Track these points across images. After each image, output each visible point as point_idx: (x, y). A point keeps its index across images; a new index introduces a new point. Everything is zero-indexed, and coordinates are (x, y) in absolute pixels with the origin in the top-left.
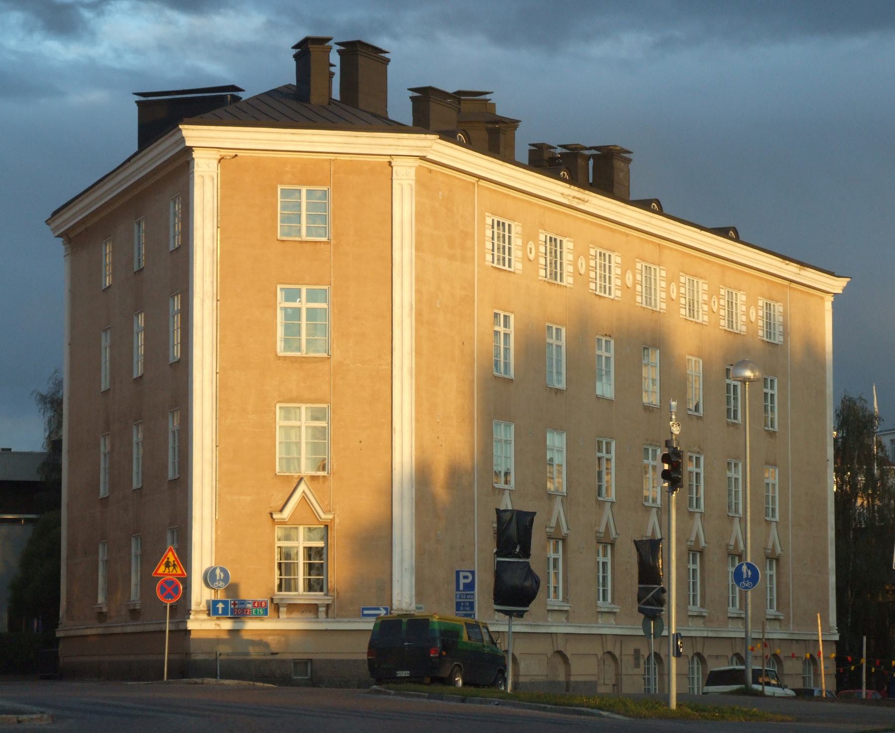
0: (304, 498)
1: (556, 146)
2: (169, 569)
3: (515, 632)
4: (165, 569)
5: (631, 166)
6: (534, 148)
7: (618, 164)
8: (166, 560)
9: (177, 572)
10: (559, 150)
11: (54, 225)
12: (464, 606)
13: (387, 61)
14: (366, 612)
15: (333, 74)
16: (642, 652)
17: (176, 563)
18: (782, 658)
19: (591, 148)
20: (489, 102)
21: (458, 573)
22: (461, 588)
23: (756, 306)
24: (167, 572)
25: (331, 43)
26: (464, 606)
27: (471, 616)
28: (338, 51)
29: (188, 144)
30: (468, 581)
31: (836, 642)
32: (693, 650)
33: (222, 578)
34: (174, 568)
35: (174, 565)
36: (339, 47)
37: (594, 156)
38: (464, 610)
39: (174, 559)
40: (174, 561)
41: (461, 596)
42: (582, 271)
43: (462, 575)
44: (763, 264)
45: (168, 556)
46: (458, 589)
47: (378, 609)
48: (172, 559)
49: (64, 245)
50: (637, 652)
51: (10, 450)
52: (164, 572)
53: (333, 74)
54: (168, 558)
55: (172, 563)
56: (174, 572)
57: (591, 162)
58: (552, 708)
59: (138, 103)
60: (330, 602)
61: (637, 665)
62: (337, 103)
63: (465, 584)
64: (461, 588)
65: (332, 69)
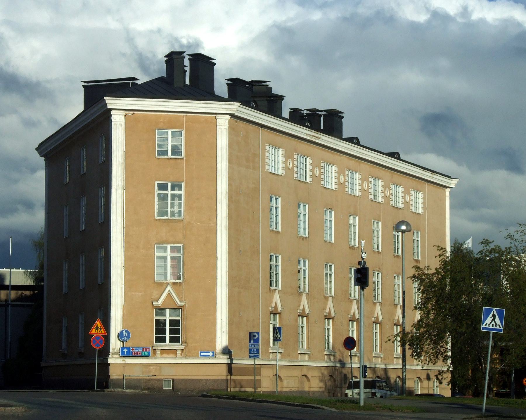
0: (169, 294)
2: (97, 331)
4: (96, 331)
8: (96, 326)
9: (102, 332)
10: (305, 112)
12: (254, 351)
14: (202, 354)
15: (186, 71)
17: (101, 327)
19: (322, 111)
20: (268, 86)
25: (185, 54)
26: (254, 351)
27: (257, 356)
29: (109, 107)
33: (126, 336)
35: (100, 329)
36: (189, 57)
37: (324, 115)
38: (254, 353)
40: (100, 327)
41: (252, 346)
47: (208, 352)
48: (99, 325)
52: (95, 332)
55: (99, 327)
56: (100, 332)
57: (322, 118)
59: (84, 86)
60: (183, 348)
65: (186, 69)
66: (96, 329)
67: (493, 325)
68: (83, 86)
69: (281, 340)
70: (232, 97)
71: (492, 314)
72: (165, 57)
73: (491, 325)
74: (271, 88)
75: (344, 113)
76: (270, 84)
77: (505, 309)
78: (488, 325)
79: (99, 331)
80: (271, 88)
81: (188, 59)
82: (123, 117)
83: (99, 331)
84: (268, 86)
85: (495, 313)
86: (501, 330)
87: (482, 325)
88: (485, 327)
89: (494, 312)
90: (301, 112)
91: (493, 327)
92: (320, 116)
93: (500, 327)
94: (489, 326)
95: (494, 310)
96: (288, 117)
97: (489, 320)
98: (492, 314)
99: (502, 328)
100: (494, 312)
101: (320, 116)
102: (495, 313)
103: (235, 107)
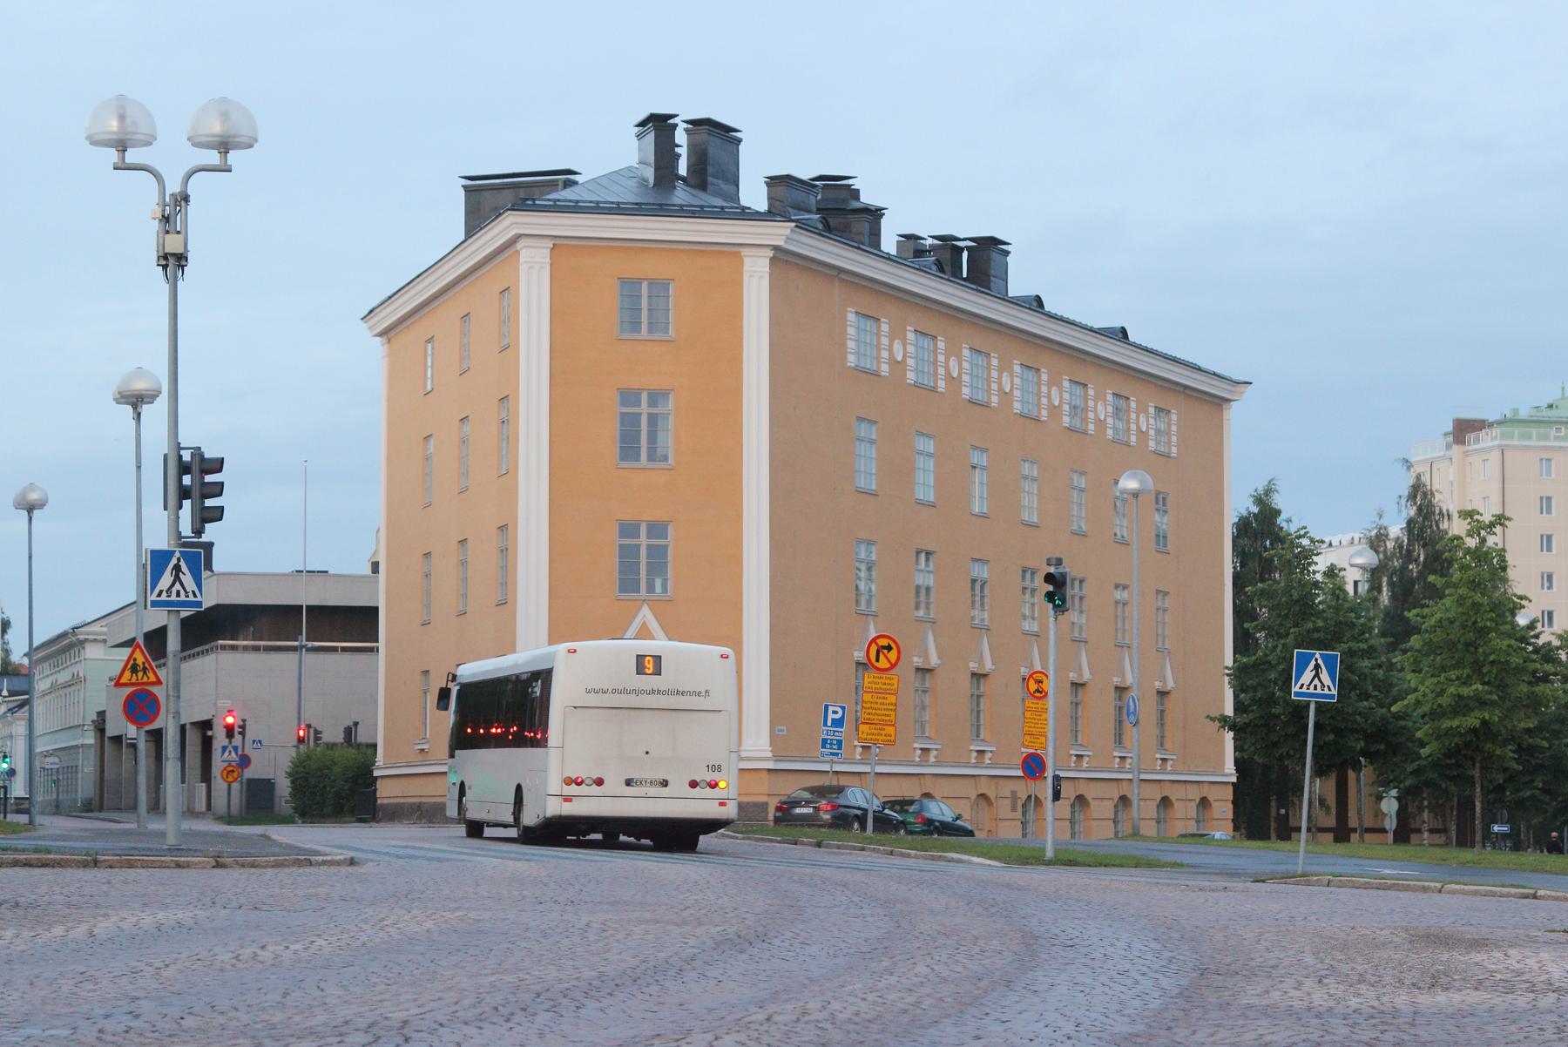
1: (926, 236)
2: (137, 676)
3: (837, 772)
4: (132, 676)
5: (1009, 259)
6: (903, 239)
7: (995, 256)
8: (132, 662)
9: (149, 679)
10: (930, 241)
11: (371, 323)
12: (831, 744)
13: (739, 141)
15: (679, 155)
16: (1019, 795)
17: (146, 665)
18: (1212, 801)
20: (853, 187)
21: (827, 707)
22: (829, 723)
23: (1105, 401)
24: (134, 680)
28: (686, 130)
30: (837, 716)
31: (1233, 783)
32: (1075, 791)
34: (145, 673)
35: (145, 670)
36: (686, 125)
37: (968, 248)
38: (831, 748)
39: (143, 660)
40: (144, 663)
42: (1144, 429)
43: (831, 709)
44: (860, 265)
45: (134, 656)
46: (825, 724)
49: (383, 345)
50: (1014, 793)
51: (327, 572)
53: (679, 155)
54: (135, 660)
55: (142, 666)
56: (145, 679)
57: (965, 255)
58: (916, 855)
59: (465, 187)
61: (1014, 809)
62: (894, 258)
63: (833, 720)
64: (829, 723)
65: (678, 150)
66: (132, 672)
67: (178, 592)
68: (463, 186)
69: (201, 602)
70: (774, 213)
71: (1313, 663)
72: (638, 126)
73: (1312, 686)
74: (858, 191)
75: (678, 115)
76: (856, 184)
77: (1296, 651)
78: (164, 594)
79: (140, 677)
80: (858, 191)
81: (685, 129)
82: (548, 251)
83: (140, 677)
84: (853, 187)
85: (1320, 661)
86: (1332, 697)
87: (1295, 685)
88: (1301, 690)
89: (1316, 660)
90: (922, 241)
91: (178, 599)
92: (962, 249)
93: (1330, 690)
94: (1308, 689)
95: (1317, 656)
96: (893, 252)
97: (1308, 676)
98: (1313, 663)
99: (1334, 692)
100: (1316, 660)
101: (962, 249)
102: (1320, 661)
103: (779, 233)
